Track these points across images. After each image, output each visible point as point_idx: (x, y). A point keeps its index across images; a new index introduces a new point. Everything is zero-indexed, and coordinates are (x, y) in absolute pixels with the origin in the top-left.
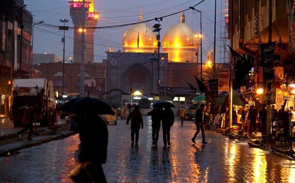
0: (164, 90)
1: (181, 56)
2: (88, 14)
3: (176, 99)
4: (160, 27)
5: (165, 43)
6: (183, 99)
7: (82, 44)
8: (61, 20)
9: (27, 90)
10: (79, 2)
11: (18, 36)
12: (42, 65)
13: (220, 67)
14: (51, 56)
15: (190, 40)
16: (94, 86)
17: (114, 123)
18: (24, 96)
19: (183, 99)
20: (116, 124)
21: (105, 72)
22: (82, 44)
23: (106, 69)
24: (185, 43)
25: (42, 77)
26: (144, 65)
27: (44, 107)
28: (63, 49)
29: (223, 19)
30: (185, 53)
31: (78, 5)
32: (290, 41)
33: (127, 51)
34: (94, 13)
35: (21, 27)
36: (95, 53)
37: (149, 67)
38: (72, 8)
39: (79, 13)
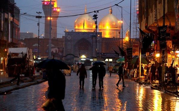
0: (99, 54)
1: (110, 34)
2: (53, 9)
3: (107, 60)
4: (97, 17)
5: (100, 26)
6: (111, 60)
7: (50, 27)
8: (37, 12)
9: (17, 54)
10: (48, 1)
11: (11, 22)
12: (26, 39)
13: (134, 41)
14: (31, 34)
15: (115, 24)
16: (57, 52)
17: (69, 75)
18: (15, 58)
19: (111, 60)
20: (70, 75)
21: (64, 44)
22: (50, 27)
23: (64, 42)
24: (112, 26)
25: (25, 47)
26: (87, 39)
27: (26, 65)
28: (38, 30)
29: (135, 12)
30: (112, 32)
31: (48, 3)
32: (176, 25)
33: (77, 31)
34: (57, 8)
35: (13, 16)
36: (58, 32)
37: (90, 41)
38: (44, 5)
39: (48, 8)
